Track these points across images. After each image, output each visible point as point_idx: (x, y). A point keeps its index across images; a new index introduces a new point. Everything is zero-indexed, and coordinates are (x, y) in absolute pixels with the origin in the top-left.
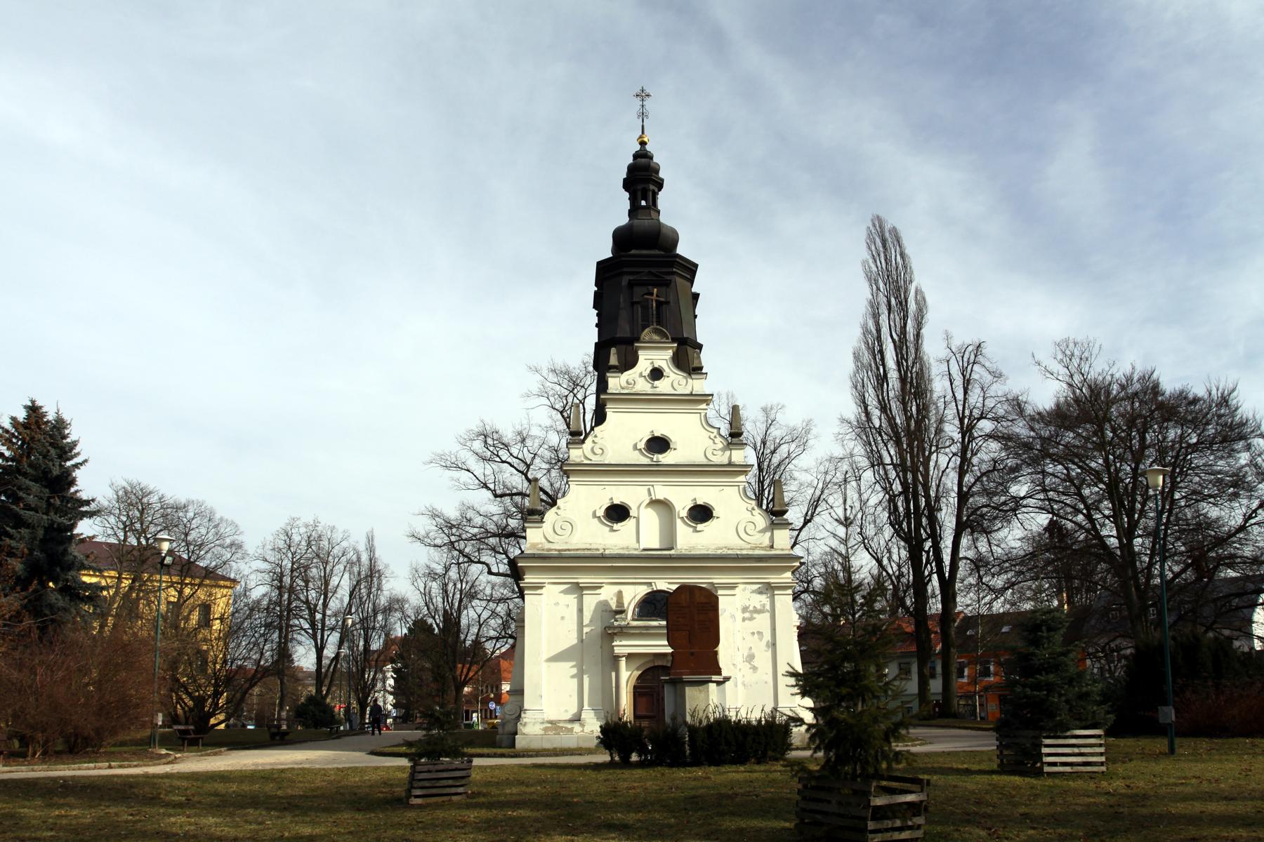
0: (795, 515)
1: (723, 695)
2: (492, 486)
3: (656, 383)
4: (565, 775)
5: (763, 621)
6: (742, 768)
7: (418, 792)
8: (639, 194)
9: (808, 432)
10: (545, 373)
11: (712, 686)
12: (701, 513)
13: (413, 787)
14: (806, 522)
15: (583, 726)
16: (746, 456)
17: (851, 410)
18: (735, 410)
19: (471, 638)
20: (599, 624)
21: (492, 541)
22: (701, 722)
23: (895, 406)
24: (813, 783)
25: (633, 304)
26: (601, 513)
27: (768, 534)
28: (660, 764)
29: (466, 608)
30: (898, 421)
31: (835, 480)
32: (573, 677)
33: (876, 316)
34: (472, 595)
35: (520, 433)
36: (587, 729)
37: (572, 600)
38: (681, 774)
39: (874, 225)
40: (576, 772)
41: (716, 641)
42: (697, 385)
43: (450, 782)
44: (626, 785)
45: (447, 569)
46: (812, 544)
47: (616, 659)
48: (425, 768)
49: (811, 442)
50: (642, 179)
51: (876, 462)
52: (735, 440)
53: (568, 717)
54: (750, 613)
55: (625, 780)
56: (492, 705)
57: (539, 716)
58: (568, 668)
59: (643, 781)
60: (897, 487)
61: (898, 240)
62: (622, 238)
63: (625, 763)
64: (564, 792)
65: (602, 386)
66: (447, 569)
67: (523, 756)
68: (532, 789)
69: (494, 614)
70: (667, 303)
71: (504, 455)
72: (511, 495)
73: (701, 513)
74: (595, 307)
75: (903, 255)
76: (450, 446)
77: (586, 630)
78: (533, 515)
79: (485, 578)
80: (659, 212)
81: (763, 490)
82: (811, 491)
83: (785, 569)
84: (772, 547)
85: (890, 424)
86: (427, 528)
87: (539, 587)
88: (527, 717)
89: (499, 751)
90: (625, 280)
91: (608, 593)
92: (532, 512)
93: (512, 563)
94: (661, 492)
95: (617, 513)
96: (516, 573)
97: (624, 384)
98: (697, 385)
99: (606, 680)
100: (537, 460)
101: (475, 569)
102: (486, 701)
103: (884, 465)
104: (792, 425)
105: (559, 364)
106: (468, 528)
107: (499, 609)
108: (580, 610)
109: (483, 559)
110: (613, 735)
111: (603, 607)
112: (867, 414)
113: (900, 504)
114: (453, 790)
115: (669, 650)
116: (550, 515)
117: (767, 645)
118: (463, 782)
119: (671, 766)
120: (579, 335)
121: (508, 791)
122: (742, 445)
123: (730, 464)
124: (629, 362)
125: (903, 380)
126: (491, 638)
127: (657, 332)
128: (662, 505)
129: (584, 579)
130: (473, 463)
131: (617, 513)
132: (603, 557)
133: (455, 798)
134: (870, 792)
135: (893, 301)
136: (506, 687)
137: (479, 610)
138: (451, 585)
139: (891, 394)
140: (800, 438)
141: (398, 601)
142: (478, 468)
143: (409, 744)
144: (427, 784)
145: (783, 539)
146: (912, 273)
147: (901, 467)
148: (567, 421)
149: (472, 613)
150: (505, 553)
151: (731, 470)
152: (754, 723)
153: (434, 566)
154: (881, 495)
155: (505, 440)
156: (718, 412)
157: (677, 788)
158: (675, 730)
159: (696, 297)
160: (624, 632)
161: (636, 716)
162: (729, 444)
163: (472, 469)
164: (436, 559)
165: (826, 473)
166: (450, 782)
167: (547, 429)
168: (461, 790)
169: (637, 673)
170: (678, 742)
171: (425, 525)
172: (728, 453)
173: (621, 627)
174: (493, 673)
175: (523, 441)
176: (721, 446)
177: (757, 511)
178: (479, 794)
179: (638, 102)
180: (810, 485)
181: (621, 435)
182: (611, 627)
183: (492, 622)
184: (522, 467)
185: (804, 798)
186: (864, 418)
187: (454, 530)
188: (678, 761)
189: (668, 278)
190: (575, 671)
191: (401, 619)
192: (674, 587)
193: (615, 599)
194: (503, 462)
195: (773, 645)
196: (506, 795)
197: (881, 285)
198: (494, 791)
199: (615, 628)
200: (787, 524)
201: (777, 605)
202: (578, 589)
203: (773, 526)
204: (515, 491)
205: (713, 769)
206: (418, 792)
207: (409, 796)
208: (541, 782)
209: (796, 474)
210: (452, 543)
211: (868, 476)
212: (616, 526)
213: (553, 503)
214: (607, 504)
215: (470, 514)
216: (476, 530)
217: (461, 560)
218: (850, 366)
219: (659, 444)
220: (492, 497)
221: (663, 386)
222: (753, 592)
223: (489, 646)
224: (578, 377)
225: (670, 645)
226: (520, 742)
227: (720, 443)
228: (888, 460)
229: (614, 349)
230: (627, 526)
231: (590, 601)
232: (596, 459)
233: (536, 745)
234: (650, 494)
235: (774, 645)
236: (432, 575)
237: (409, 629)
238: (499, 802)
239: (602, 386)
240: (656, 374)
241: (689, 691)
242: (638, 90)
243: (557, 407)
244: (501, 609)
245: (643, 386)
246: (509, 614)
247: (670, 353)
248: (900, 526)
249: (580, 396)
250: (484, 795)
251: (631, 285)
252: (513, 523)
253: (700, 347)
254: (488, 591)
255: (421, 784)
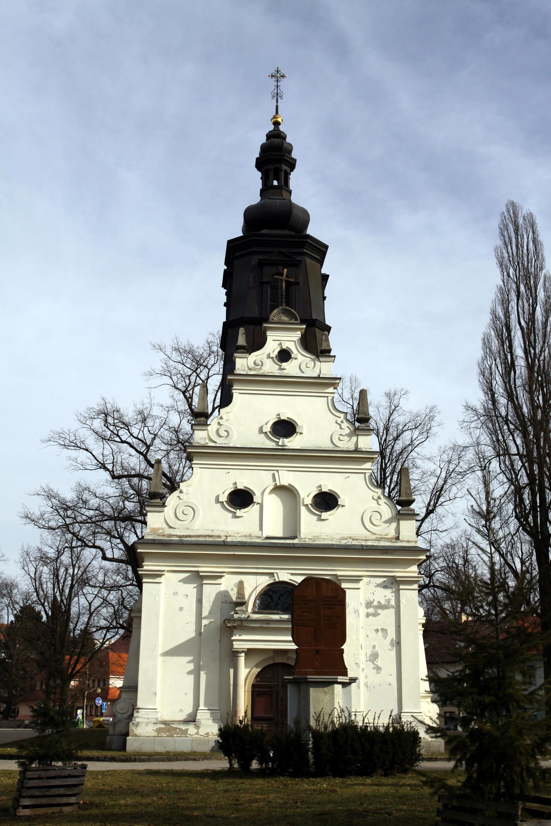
0: (419, 506)
1: (348, 697)
2: (110, 467)
3: (284, 365)
4: (181, 784)
5: (387, 618)
6: (369, 781)
7: (26, 802)
8: (271, 174)
9: (431, 419)
10: (169, 351)
11: (338, 688)
12: (326, 501)
13: (21, 796)
14: (429, 513)
15: (197, 727)
16: (369, 443)
17: (478, 398)
18: (363, 393)
19: (81, 626)
20: (218, 615)
21: (108, 524)
22: (326, 727)
23: (522, 397)
24: (455, 803)
25: (262, 284)
26: (224, 498)
27: (394, 525)
28: (282, 774)
29: (77, 595)
30: (525, 410)
31: (458, 469)
32: (189, 673)
33: (505, 303)
34: (83, 581)
35: (141, 413)
36: (202, 731)
37: (191, 589)
38: (304, 786)
39: (508, 211)
40: (193, 780)
41: (343, 640)
42: (325, 368)
43: (62, 791)
44: (247, 796)
45: (59, 553)
46: (434, 536)
47: (235, 654)
48: (36, 774)
49: (434, 430)
50: (275, 159)
51: (502, 452)
52: (363, 426)
53: (183, 717)
54: (374, 608)
55: (246, 791)
56: (99, 702)
57: (152, 716)
58: (184, 664)
59: (264, 793)
60: (524, 480)
61: (533, 225)
62: (253, 218)
63: (245, 772)
64: (182, 804)
65: (229, 366)
66: (59, 553)
67: (135, 761)
68: (148, 800)
69: (105, 602)
70: (296, 283)
71: (124, 434)
72: (129, 476)
73: (326, 501)
74: (224, 286)
75: (535, 241)
76: (71, 425)
77: (205, 622)
78: (156, 499)
79: (98, 563)
80: (290, 192)
81: (385, 478)
82: (434, 480)
83: (410, 563)
84: (398, 538)
85: (516, 413)
86: (42, 509)
87: (158, 575)
88: (140, 717)
89: (110, 754)
90: (255, 260)
91: (228, 584)
92: (153, 495)
93: (131, 550)
94: (287, 477)
95: (241, 499)
96: (133, 557)
97: (251, 365)
98: (325, 368)
99: (224, 677)
100: (157, 441)
101: (88, 553)
102: (92, 697)
103: (510, 455)
104: (415, 411)
105: (183, 344)
106: (83, 511)
107: (111, 597)
108: (200, 601)
109: (98, 543)
110: (231, 739)
111: (223, 598)
112: (494, 401)
113: (525, 496)
114: (65, 800)
115: (294, 647)
116: (172, 500)
117: (392, 644)
118: (76, 791)
119: (294, 775)
120: (205, 312)
121: (122, 802)
122: (368, 431)
123: (357, 451)
124: (257, 343)
125: (530, 367)
126: (102, 628)
127: (286, 312)
128: (286, 492)
129: (205, 568)
130: (92, 442)
131: (241, 499)
132: (225, 545)
133: (66, 809)
134: (516, 815)
135: (522, 288)
136: (116, 683)
137: (90, 597)
138: (62, 570)
139: (519, 382)
140: (423, 425)
141: (7, 585)
142: (97, 447)
143: (20, 744)
144: (36, 792)
145: (408, 528)
146: (543, 260)
147: (527, 457)
148: (189, 400)
149: (83, 601)
150: (121, 537)
151: (356, 456)
152: (381, 729)
153: (46, 549)
154: (506, 486)
155: (126, 419)
156: (341, 396)
157: (302, 802)
158: (298, 736)
159: (325, 278)
160: (244, 625)
161: (254, 718)
162: (356, 429)
163: (90, 448)
164: (48, 542)
165: (449, 462)
166: (62, 791)
167: (169, 409)
168: (72, 800)
169: (256, 671)
170: (302, 748)
171: (40, 506)
172: (354, 439)
173: (241, 620)
174: (101, 666)
175: (144, 420)
176: (347, 431)
177: (383, 500)
178: (92, 805)
179: (272, 82)
180: (432, 474)
181: (247, 418)
182: (231, 620)
183: (104, 611)
184: (143, 449)
185: (444, 820)
186: (491, 406)
187: (69, 513)
188: (301, 771)
189: (298, 258)
190: (191, 667)
191: (8, 606)
192: (299, 579)
193: (235, 590)
194: (123, 442)
195: (398, 643)
196: (120, 806)
197: (511, 271)
198: (107, 801)
199: (235, 620)
200: (412, 515)
201: (403, 600)
202: (198, 578)
203: (399, 516)
204: (133, 473)
205: (338, 780)
206: (26, 802)
207: (16, 805)
208: (157, 792)
209: (419, 462)
210: (67, 526)
211: (495, 466)
212: (239, 513)
213: (173, 486)
214: (230, 489)
215: (86, 496)
216: (91, 513)
217: (74, 544)
218: (479, 353)
219: (285, 428)
220: (109, 478)
221: (290, 368)
222: (378, 585)
223: (98, 636)
224: (202, 357)
225: (294, 641)
226: (132, 745)
227: (346, 428)
228: (514, 450)
229: (242, 328)
230: (249, 514)
231: (210, 592)
232: (221, 442)
233: (148, 748)
234: (274, 480)
235: (399, 643)
236: (44, 559)
237: (16, 616)
238: (114, 815)
239: (229, 366)
240: (284, 355)
241: (314, 692)
242: (273, 71)
243: (180, 386)
244: (113, 597)
245: (270, 368)
246: (122, 602)
247: (299, 334)
248: (526, 519)
249: (203, 376)
250: (97, 806)
251: (261, 264)
252: (130, 506)
253: (328, 329)
254: (101, 578)
255: (30, 792)
